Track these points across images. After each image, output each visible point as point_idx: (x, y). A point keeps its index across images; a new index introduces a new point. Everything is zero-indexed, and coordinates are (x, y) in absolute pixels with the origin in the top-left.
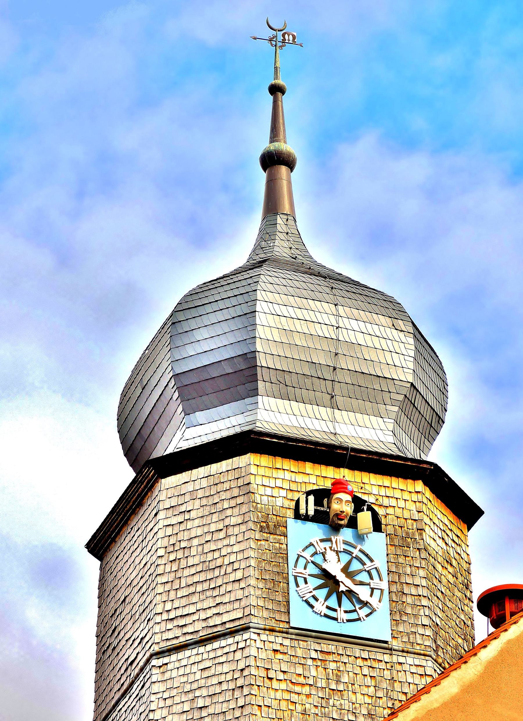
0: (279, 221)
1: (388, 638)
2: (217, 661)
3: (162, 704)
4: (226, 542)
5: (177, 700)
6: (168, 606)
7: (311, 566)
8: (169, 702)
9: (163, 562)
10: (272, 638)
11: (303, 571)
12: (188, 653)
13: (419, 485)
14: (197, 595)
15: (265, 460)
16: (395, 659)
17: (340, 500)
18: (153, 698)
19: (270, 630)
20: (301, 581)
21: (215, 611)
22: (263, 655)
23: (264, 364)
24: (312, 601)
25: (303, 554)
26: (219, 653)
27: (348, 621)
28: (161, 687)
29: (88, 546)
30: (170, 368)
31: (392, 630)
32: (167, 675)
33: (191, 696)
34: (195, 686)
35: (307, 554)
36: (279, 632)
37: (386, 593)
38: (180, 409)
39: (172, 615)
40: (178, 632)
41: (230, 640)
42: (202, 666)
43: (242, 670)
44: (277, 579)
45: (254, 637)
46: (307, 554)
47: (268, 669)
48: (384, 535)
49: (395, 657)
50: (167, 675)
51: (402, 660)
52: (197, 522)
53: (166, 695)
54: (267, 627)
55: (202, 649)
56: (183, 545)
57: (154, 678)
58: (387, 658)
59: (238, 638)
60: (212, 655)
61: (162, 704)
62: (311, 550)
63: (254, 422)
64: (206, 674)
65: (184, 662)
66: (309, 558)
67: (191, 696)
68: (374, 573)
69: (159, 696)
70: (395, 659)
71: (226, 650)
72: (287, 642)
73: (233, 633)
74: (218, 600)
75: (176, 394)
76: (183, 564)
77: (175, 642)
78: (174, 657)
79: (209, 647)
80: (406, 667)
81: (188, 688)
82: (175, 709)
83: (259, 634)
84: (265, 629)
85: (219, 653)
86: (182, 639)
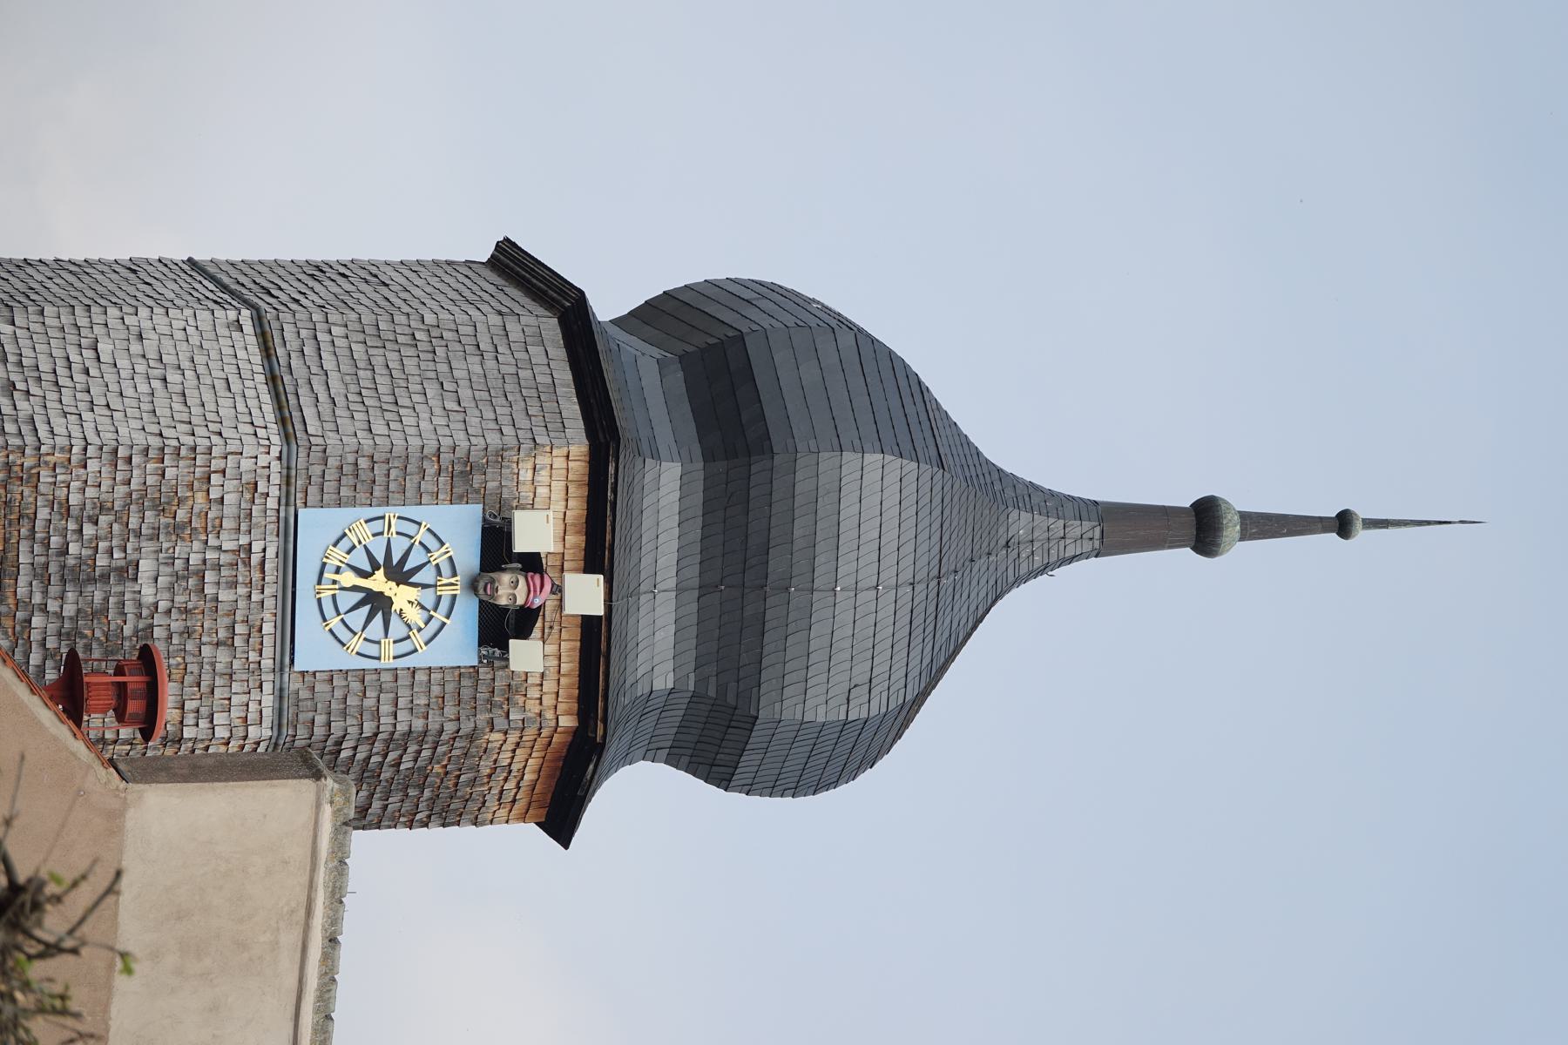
0: (1087, 525)
1: (298, 667)
2: (239, 399)
3: (178, 324)
4: (438, 411)
5: (183, 346)
6: (336, 330)
7: (406, 542)
8: (179, 335)
9: (413, 324)
10: (275, 479)
11: (393, 529)
12: (257, 359)
13: (568, 722)
14: (353, 371)
15: (579, 467)
16: (267, 677)
17: (515, 584)
18: (188, 312)
19: (288, 477)
20: (377, 526)
21: (323, 397)
22: (246, 464)
23: (754, 469)
24: (345, 544)
25: (423, 530)
26: (252, 403)
27: (319, 600)
28: (205, 325)
29: (507, 240)
30: (755, 327)
31: (314, 673)
32: (222, 331)
33: (186, 364)
34: (201, 370)
35: (422, 535)
36: (288, 493)
37: (372, 664)
38: (690, 349)
39: (321, 336)
40: (293, 344)
41: (270, 417)
42: (233, 379)
43: (220, 434)
44: (364, 482)
45: (275, 451)
46: (422, 535)
47: (224, 472)
48: (475, 663)
49: (271, 677)
50: (222, 331)
51: (267, 687)
52: (477, 369)
53: (190, 330)
54: (293, 473)
55: (261, 378)
56: (440, 352)
57: (219, 313)
58: (267, 663)
59: (274, 428)
60: (250, 393)
61: (178, 324)
62: (431, 542)
63: (656, 455)
64: (220, 385)
65: (241, 354)
66: (418, 538)
67: (186, 364)
68: (405, 647)
69: (191, 321)
70: (267, 677)
71: (255, 412)
72: (272, 503)
73: (283, 421)
74: (340, 401)
75: (712, 341)
76: (406, 351)
77: (277, 340)
78: (252, 340)
79: (263, 389)
80: (255, 695)
81: (199, 359)
82: (167, 342)
83: (280, 458)
84: (288, 468)
85: (252, 403)
86: (280, 351)
